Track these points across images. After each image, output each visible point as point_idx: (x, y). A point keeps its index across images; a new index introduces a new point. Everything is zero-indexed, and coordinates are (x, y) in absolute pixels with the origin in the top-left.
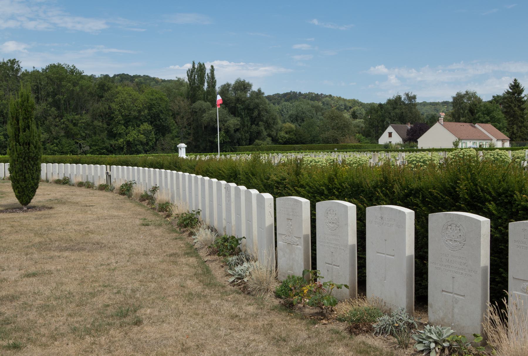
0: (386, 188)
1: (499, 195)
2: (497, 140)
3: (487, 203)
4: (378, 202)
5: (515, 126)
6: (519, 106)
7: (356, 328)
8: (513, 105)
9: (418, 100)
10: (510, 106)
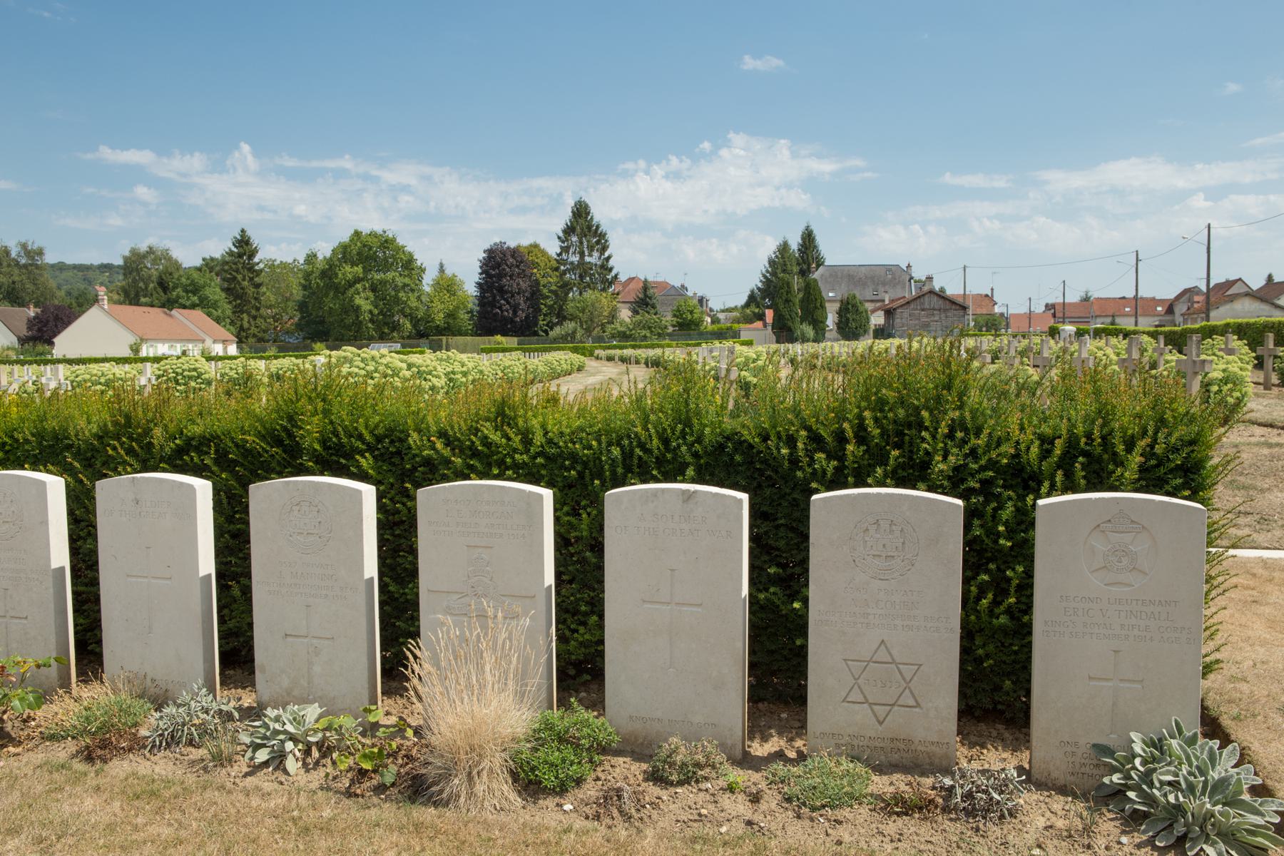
0: (131, 438)
1: (379, 439)
2: (215, 342)
3: (358, 457)
4: (112, 467)
5: (245, 316)
6: (251, 279)
7: (103, 747)
8: (239, 277)
9: (50, 258)
10: (235, 278)
